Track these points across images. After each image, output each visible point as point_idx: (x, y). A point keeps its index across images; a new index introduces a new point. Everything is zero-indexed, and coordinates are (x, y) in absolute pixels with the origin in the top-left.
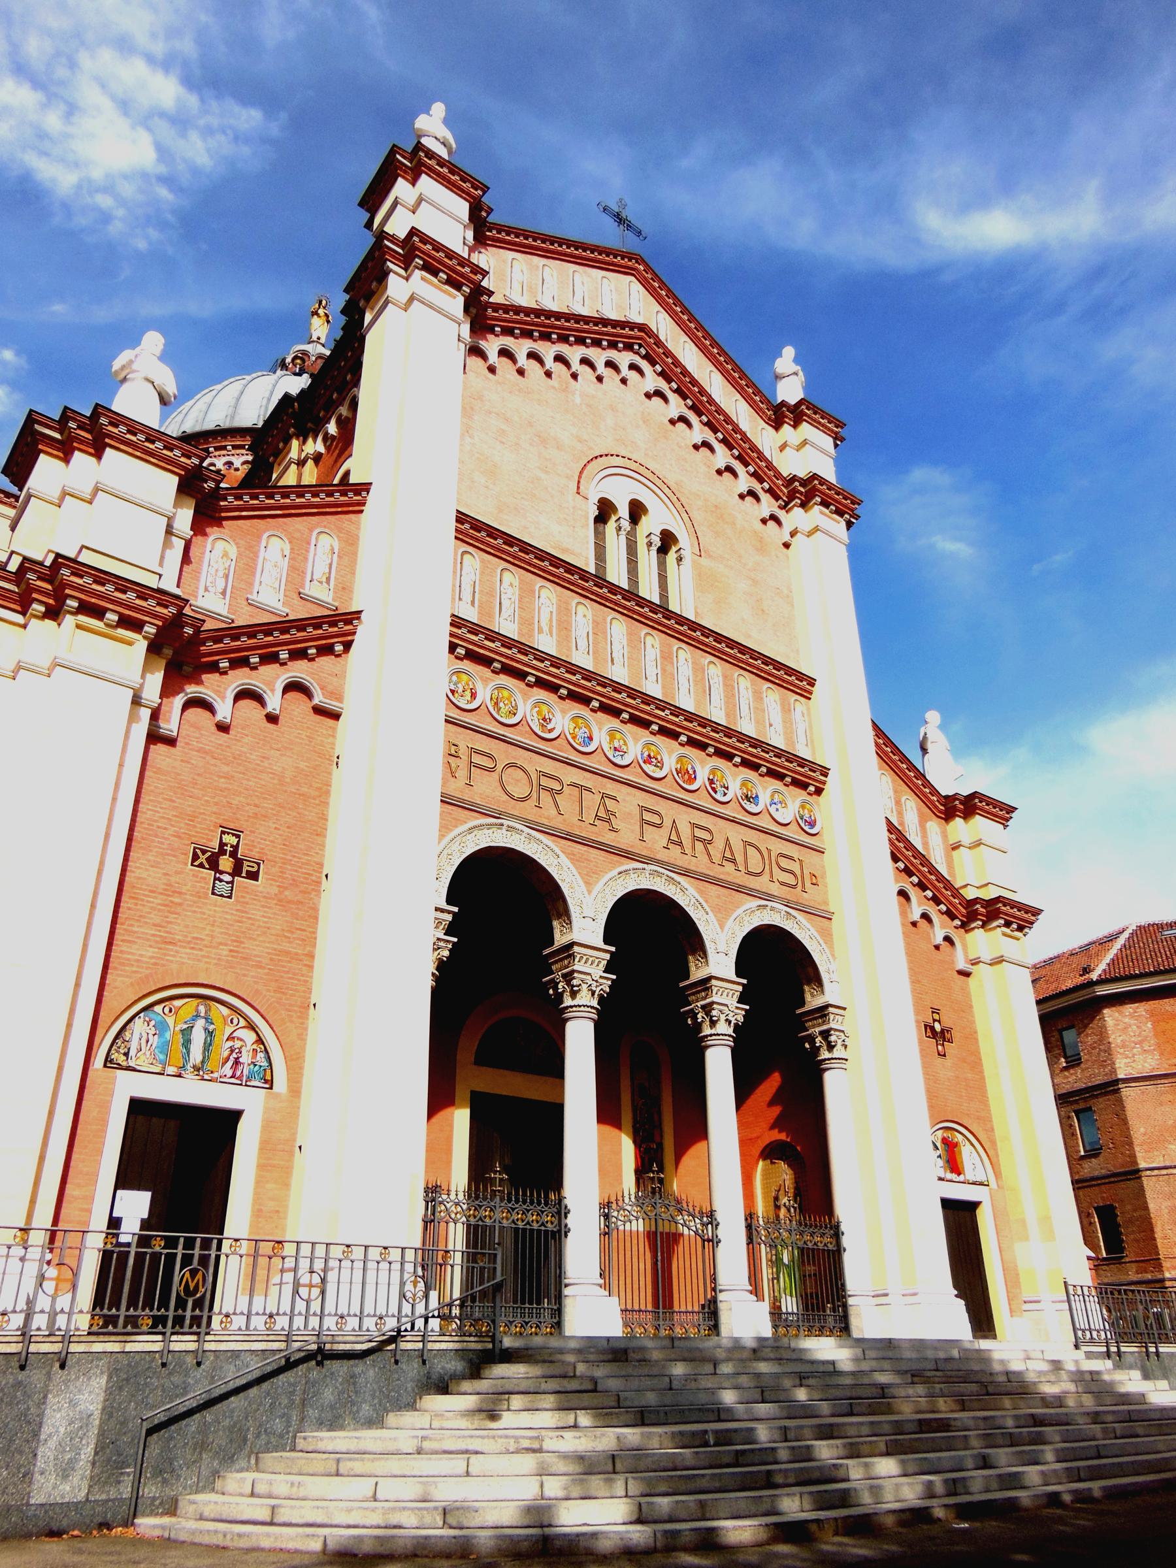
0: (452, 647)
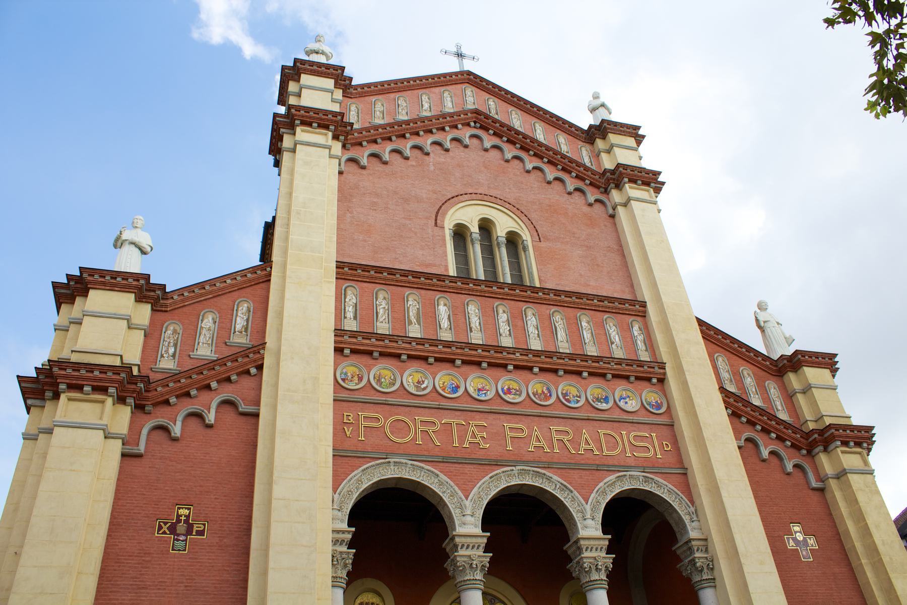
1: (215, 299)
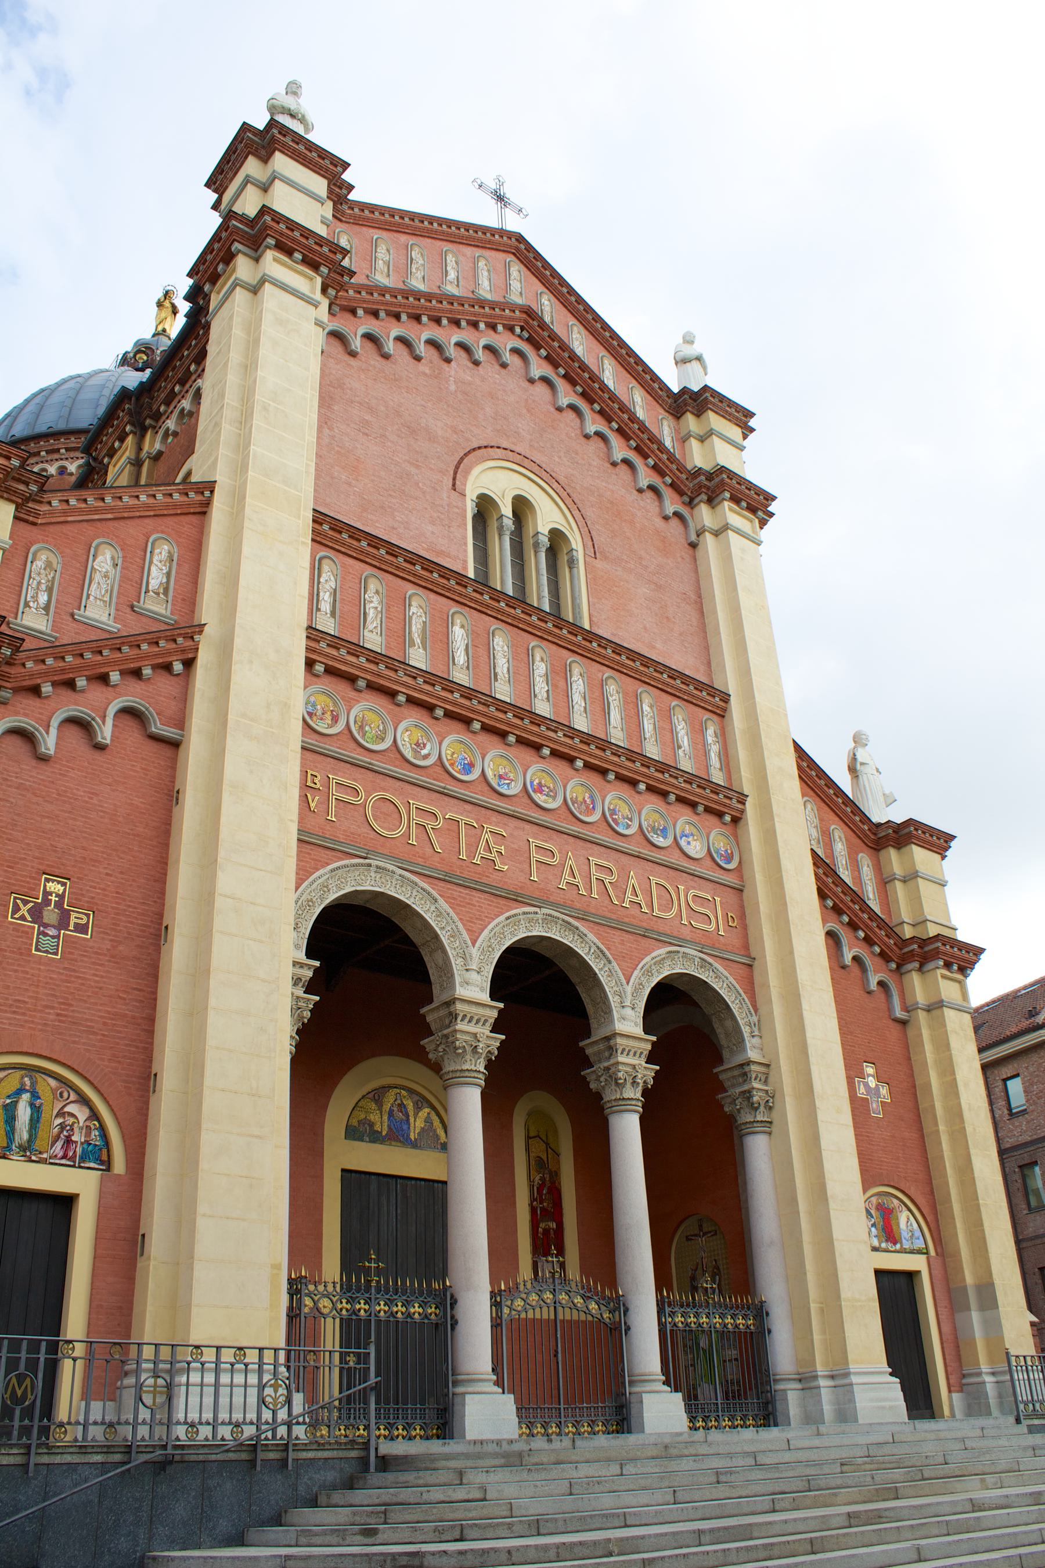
0: (310, 664)
1: (116, 524)
